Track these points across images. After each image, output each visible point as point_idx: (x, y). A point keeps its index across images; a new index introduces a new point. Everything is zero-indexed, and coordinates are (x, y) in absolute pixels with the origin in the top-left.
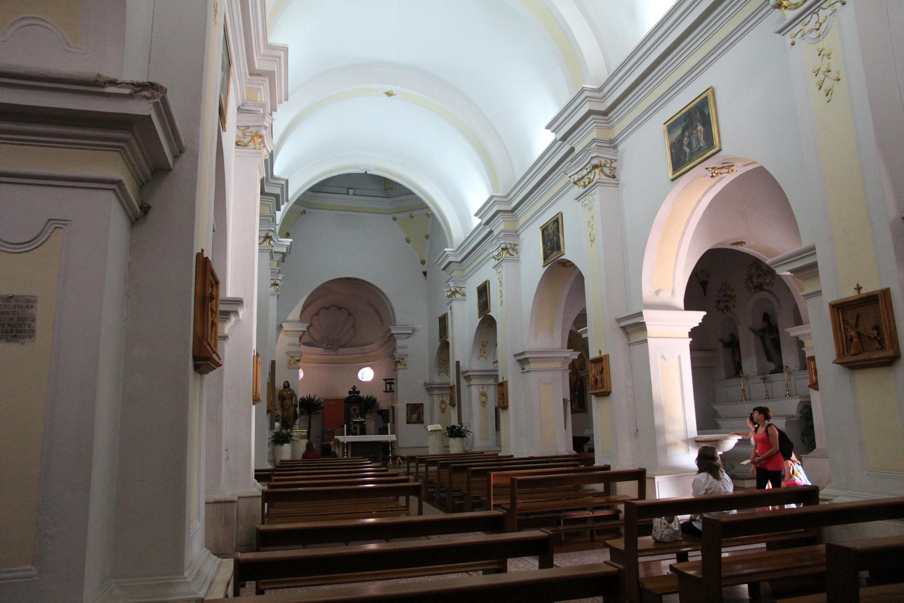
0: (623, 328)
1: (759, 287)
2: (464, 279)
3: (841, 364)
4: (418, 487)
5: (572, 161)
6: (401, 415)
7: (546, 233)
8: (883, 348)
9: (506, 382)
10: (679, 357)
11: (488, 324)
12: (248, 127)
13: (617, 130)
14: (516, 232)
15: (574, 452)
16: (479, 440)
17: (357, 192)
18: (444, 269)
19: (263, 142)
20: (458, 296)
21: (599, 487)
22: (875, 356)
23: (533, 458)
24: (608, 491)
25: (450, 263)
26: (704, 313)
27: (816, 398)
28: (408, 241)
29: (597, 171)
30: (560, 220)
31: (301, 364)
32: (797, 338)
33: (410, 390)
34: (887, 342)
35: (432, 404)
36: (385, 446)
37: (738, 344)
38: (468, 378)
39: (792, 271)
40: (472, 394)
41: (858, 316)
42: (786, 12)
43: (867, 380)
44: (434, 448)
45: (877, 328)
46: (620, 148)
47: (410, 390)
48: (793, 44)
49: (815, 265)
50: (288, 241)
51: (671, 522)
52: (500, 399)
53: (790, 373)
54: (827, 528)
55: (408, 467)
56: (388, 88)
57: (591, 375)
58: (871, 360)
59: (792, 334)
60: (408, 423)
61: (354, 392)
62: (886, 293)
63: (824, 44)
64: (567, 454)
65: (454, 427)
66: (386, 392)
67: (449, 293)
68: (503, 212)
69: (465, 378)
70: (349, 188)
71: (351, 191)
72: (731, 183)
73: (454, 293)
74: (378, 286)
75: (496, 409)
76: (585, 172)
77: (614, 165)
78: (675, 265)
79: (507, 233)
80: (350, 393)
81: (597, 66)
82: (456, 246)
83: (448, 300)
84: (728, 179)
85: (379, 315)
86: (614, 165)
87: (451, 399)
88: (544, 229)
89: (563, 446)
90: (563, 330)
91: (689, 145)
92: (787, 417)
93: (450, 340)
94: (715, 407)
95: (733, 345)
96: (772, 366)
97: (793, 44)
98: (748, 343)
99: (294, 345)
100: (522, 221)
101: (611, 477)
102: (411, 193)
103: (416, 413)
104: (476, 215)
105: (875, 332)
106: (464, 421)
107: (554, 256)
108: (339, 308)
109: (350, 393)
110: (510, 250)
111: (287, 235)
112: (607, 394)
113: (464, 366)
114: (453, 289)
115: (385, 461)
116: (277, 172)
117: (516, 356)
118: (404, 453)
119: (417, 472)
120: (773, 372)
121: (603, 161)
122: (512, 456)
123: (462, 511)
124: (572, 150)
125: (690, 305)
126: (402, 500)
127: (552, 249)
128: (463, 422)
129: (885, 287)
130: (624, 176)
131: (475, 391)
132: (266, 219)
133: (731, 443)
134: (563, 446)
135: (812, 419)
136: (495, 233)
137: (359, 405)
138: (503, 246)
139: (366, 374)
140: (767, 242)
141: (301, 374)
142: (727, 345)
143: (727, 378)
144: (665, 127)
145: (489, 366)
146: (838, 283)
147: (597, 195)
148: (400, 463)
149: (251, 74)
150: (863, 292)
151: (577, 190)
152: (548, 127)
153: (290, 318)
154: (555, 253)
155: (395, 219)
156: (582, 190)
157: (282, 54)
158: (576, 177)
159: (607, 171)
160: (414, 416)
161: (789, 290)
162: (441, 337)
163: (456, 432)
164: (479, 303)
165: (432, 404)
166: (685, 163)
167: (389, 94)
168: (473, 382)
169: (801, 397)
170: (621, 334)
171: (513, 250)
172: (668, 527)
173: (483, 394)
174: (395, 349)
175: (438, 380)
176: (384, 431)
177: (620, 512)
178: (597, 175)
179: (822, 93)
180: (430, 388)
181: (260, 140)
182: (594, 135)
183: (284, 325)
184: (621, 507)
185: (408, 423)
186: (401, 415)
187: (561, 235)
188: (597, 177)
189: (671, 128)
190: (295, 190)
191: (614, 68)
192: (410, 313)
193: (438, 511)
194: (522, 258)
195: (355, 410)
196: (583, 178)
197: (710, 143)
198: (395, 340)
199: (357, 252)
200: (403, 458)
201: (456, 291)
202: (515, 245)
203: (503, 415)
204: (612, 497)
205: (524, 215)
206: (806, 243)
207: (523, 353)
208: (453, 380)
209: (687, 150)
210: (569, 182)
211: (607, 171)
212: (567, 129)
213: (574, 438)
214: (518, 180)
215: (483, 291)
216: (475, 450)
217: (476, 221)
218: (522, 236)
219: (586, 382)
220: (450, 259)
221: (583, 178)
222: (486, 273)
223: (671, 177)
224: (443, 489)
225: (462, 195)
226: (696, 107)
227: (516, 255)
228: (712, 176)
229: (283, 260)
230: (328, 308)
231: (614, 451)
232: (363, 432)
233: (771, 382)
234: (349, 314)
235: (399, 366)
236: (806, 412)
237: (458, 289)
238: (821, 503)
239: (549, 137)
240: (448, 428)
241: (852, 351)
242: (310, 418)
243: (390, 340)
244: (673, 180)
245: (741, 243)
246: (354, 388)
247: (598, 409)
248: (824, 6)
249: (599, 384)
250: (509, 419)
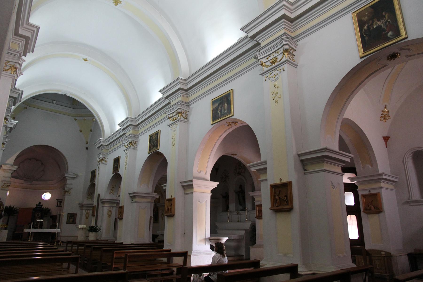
0: (183, 186)
1: (239, 174)
2: (108, 154)
3: (272, 210)
4: (77, 258)
5: (169, 108)
6: (64, 219)
7: (151, 138)
8: (287, 204)
9: (123, 206)
10: (206, 201)
11: (117, 178)
12: (9, 62)
13: (191, 98)
14: (137, 135)
15: (152, 242)
16: (104, 234)
17: (58, 103)
18: (98, 148)
19: (16, 71)
20: (103, 162)
21: (165, 259)
22: (285, 207)
23: (133, 244)
24: (169, 261)
25: (102, 145)
26: (218, 183)
27: (258, 222)
28: (81, 131)
29: (180, 115)
30: (159, 133)
31: (9, 188)
32: (252, 196)
33: (70, 205)
34: (289, 202)
35: (81, 214)
36: (54, 234)
37: (228, 197)
38: (103, 203)
39: (256, 170)
40: (104, 210)
41: (280, 191)
42: (264, 67)
43: (281, 217)
44: (81, 238)
45: (286, 196)
46: (191, 106)
47: (70, 205)
48: (265, 80)
49: (266, 169)
50: (15, 122)
51: (200, 276)
52: (119, 214)
53: (248, 211)
54: (262, 278)
55: (67, 247)
56: (85, 57)
57: (166, 206)
58: (283, 209)
59: (251, 195)
60: (67, 223)
61: (39, 205)
62: (290, 183)
63: (276, 83)
64: (149, 243)
65: (93, 226)
66: (57, 206)
67: (99, 160)
68: (132, 126)
69: (102, 202)
70: (53, 100)
71: (54, 102)
72: (235, 129)
73: (101, 160)
74: (64, 154)
75: (116, 219)
76: (174, 114)
77: (187, 113)
78: (208, 161)
79: (133, 136)
80: (37, 205)
81: (185, 69)
82: (106, 138)
83: (98, 163)
84: (235, 127)
85: (59, 166)
86: (187, 113)
87: (93, 212)
88: (151, 137)
89: (147, 239)
90: (153, 184)
91: (221, 111)
92: (246, 230)
93: (96, 183)
94: (216, 224)
95: (226, 197)
96: (241, 208)
97: (265, 80)
98: (232, 196)
99: (8, 177)
100: (140, 132)
101: (171, 255)
102: (86, 108)
103: (72, 218)
104: (119, 125)
105: (285, 198)
106: (99, 224)
107: (154, 150)
108: (37, 160)
109: (37, 205)
110: (133, 144)
111: (14, 118)
112: (172, 216)
113: (102, 197)
114: (101, 158)
115: (53, 243)
116: (17, 86)
117: (129, 194)
118: (63, 239)
119: (72, 249)
120: (241, 210)
121: (183, 111)
122: (123, 243)
123: (95, 271)
124: (169, 103)
125: (213, 179)
126: (65, 265)
127: (154, 146)
128: (98, 224)
129: (290, 180)
130: (191, 118)
131: (106, 209)
132: (9, 109)
133: (224, 240)
134: (147, 239)
135: (255, 231)
136: (127, 135)
137: (41, 211)
138: (130, 141)
139: (47, 196)
140: (244, 155)
141: (8, 194)
142: (224, 197)
143: (223, 212)
144: (211, 102)
145: (115, 198)
146: (274, 177)
147: (178, 125)
148: (60, 244)
149: (15, 35)
150: (282, 181)
151: (169, 122)
152: (160, 91)
153: (8, 162)
154: (155, 148)
155: (75, 120)
156: (172, 122)
157: (35, 30)
158: (170, 116)
159: (184, 115)
160: (71, 220)
161: (251, 176)
162: (91, 181)
163: (94, 229)
164: (114, 167)
165: (81, 214)
166: (218, 119)
167: (85, 60)
168: (106, 205)
169: (252, 222)
170: (181, 189)
171: (135, 144)
172: (199, 279)
173: (110, 211)
174: (65, 184)
175: (86, 202)
176: (54, 227)
177: (174, 271)
178: (179, 117)
179: (274, 101)
180: (81, 206)
181: (15, 70)
182: (180, 99)
183: (3, 166)
184: (175, 269)
185: (67, 223)
186: (64, 219)
187: (159, 140)
188: (179, 117)
189: (214, 102)
190: (26, 96)
191: (193, 72)
192: (77, 168)
193: (84, 271)
194: (138, 148)
195: (38, 215)
196: (173, 117)
197: (229, 112)
198: (67, 180)
199: (48, 132)
200: (62, 242)
201: (103, 159)
202: (136, 142)
203: (119, 223)
204: (171, 264)
205: (142, 129)
206: (263, 159)
207: (133, 193)
208: (95, 203)
209: (220, 113)
210: (166, 117)
211: (184, 115)
212: (168, 94)
213: (153, 235)
214: (141, 112)
215: (117, 161)
216: (102, 239)
217: (118, 128)
218: (139, 138)
219: (162, 208)
220: (102, 143)
221: (173, 117)
222: (120, 152)
223: (211, 123)
224: (86, 259)
225: (113, 115)
226: (225, 96)
227: (135, 146)
228: (228, 126)
229: (10, 131)
230: (30, 159)
231: (172, 243)
232: (41, 227)
233: (240, 214)
234: (42, 164)
235: (66, 193)
236: (253, 228)
237: (104, 159)
238: (261, 267)
239: (160, 96)
240: (89, 227)
241: (277, 205)
242: (9, 218)
243: (64, 179)
244: (212, 124)
245: (235, 154)
246: (40, 203)
247: (168, 223)
248: (277, 69)
249: (170, 211)
250: (122, 226)
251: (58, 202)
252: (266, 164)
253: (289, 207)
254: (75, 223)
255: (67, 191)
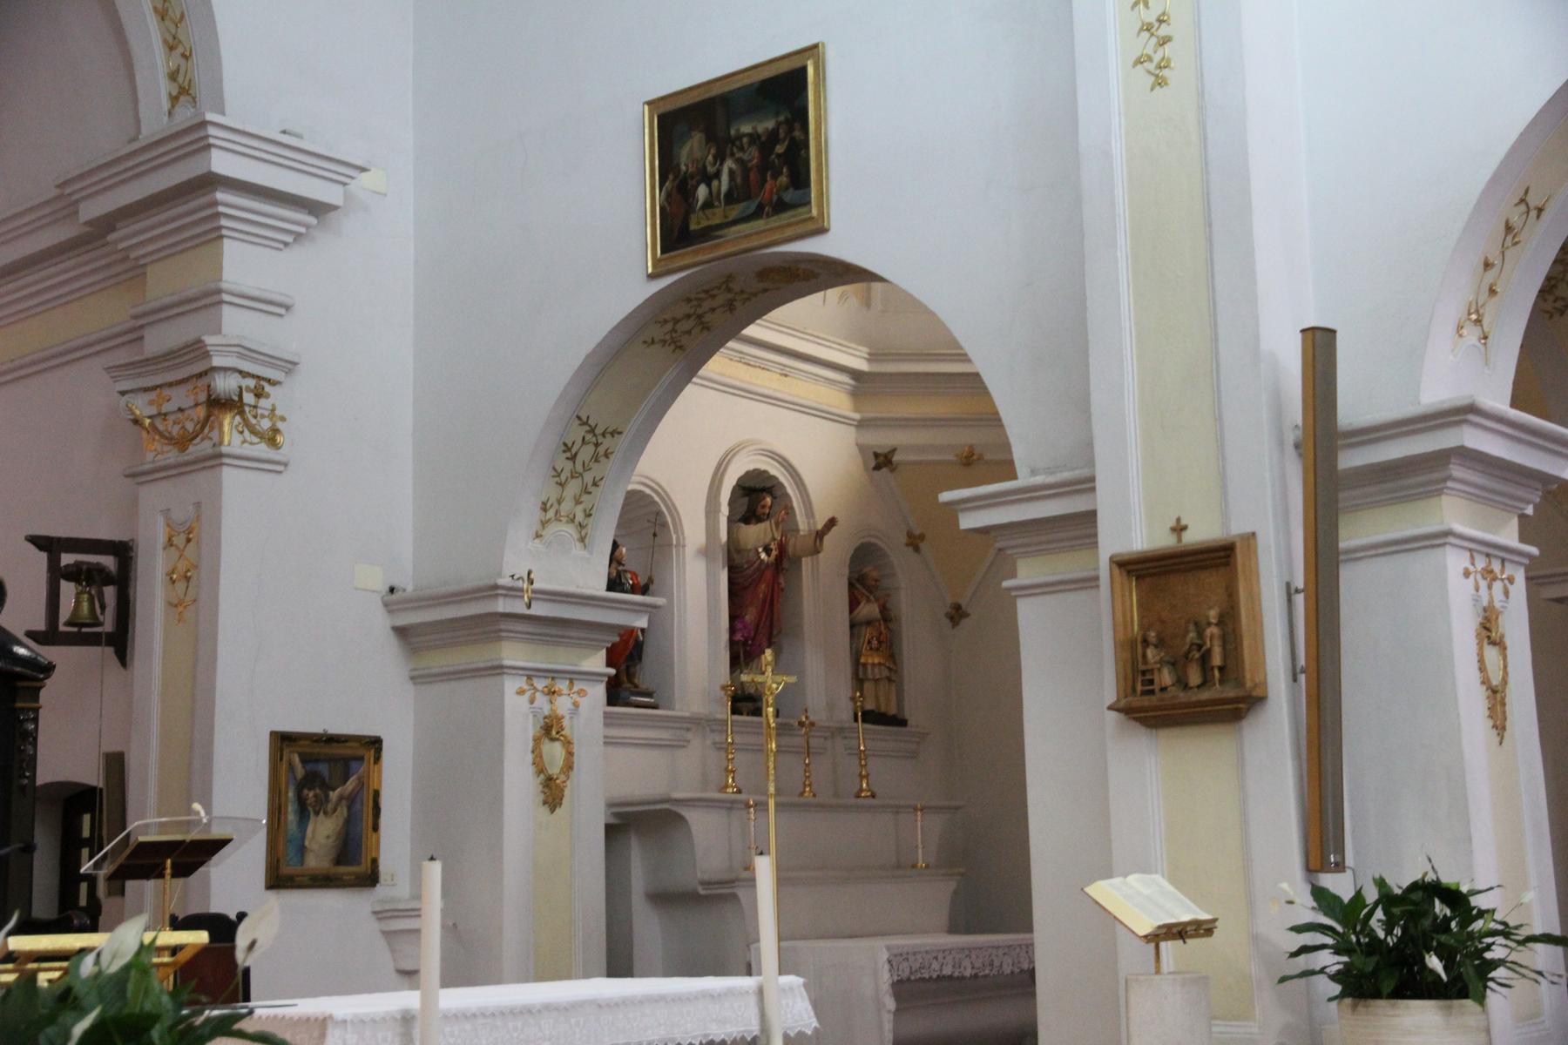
160: (322, 832)
251: (57, 574)
252: (1093, 489)
253: (363, 868)
254: (370, 879)
255: (232, 404)
